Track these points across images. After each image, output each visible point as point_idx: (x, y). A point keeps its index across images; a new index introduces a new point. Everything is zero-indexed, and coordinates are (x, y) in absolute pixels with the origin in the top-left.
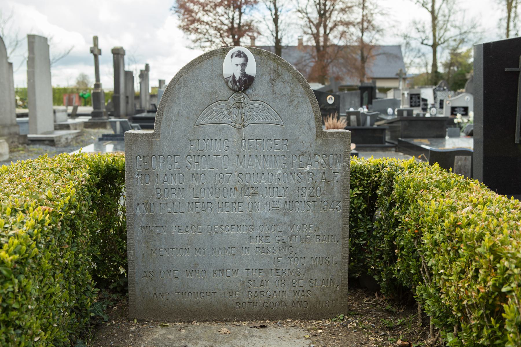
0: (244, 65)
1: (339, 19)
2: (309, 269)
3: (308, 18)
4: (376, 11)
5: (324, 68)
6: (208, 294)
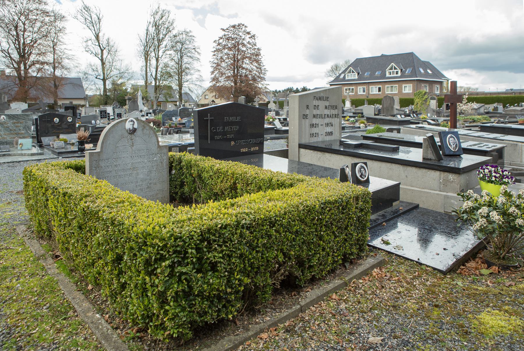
0: (133, 125)
1: (36, 59)
4: (64, 56)
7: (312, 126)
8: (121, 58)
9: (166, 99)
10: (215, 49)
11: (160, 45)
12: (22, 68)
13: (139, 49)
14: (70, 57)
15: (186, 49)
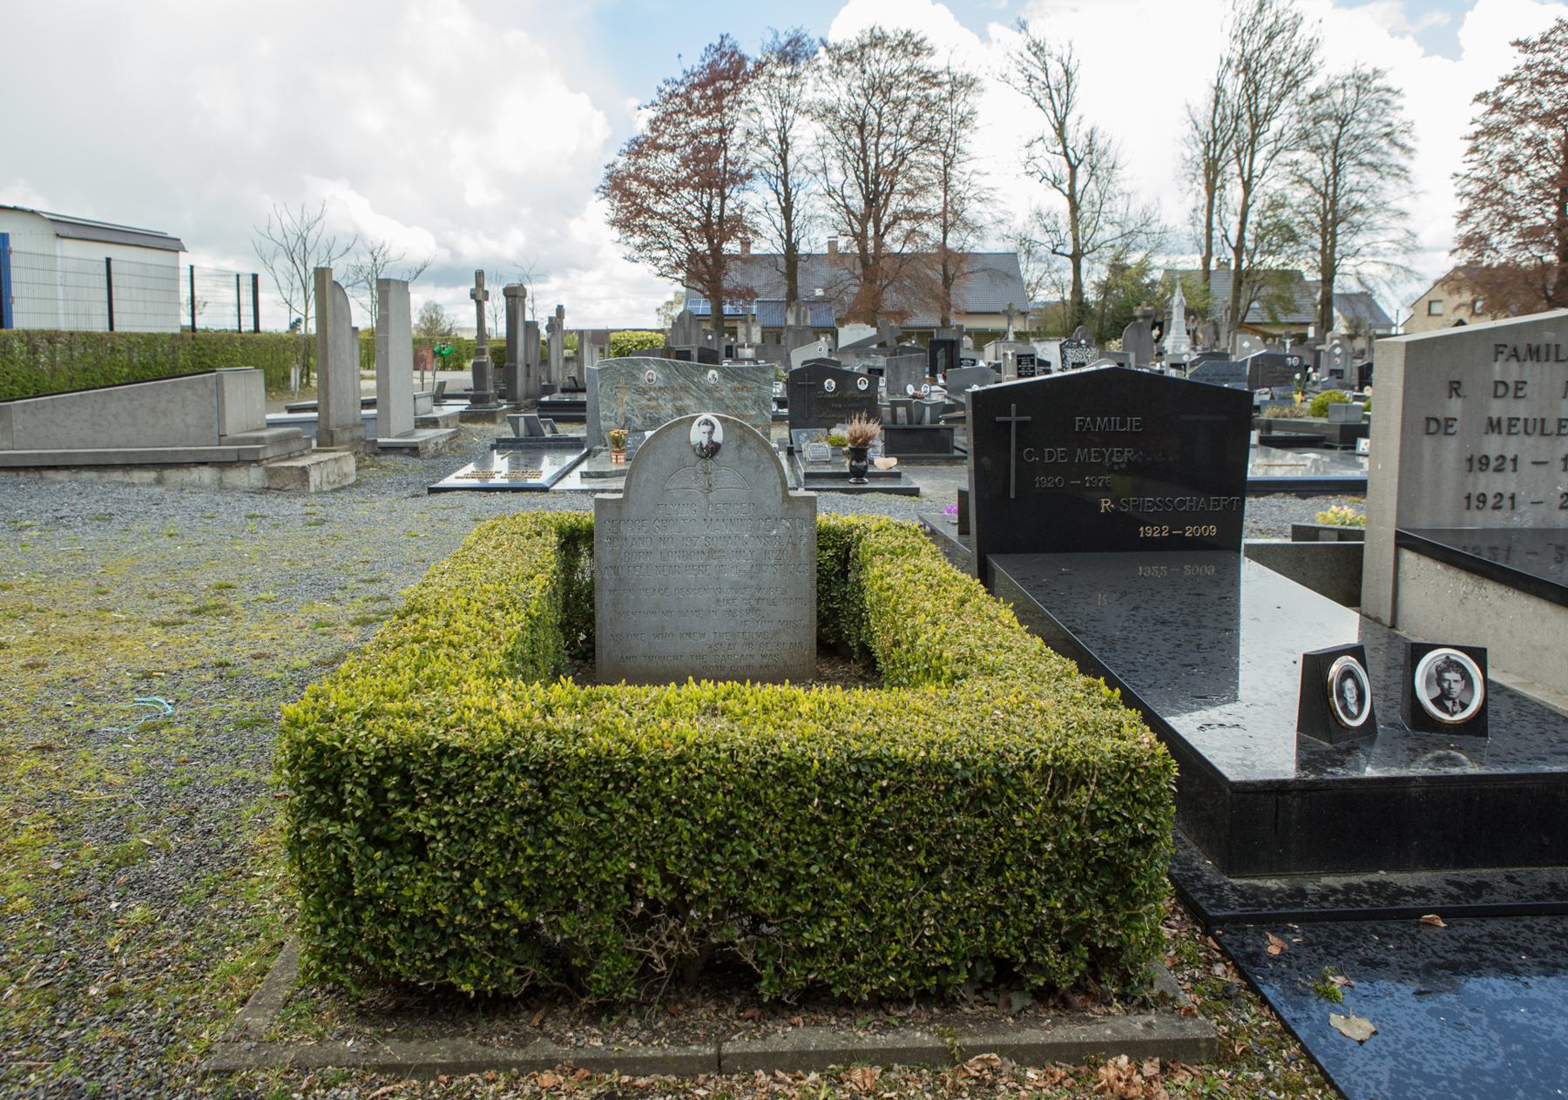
0: (711, 433)
2: (776, 633)
3: (846, 207)
5: (876, 297)
6: (676, 657)
7: (1481, 463)
8: (1126, 187)
9: (1274, 317)
10: (1478, 127)
11: (1259, 134)
12: (871, 232)
13: (1188, 155)
14: (984, 196)
15: (1357, 138)
